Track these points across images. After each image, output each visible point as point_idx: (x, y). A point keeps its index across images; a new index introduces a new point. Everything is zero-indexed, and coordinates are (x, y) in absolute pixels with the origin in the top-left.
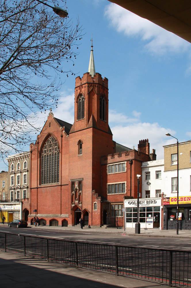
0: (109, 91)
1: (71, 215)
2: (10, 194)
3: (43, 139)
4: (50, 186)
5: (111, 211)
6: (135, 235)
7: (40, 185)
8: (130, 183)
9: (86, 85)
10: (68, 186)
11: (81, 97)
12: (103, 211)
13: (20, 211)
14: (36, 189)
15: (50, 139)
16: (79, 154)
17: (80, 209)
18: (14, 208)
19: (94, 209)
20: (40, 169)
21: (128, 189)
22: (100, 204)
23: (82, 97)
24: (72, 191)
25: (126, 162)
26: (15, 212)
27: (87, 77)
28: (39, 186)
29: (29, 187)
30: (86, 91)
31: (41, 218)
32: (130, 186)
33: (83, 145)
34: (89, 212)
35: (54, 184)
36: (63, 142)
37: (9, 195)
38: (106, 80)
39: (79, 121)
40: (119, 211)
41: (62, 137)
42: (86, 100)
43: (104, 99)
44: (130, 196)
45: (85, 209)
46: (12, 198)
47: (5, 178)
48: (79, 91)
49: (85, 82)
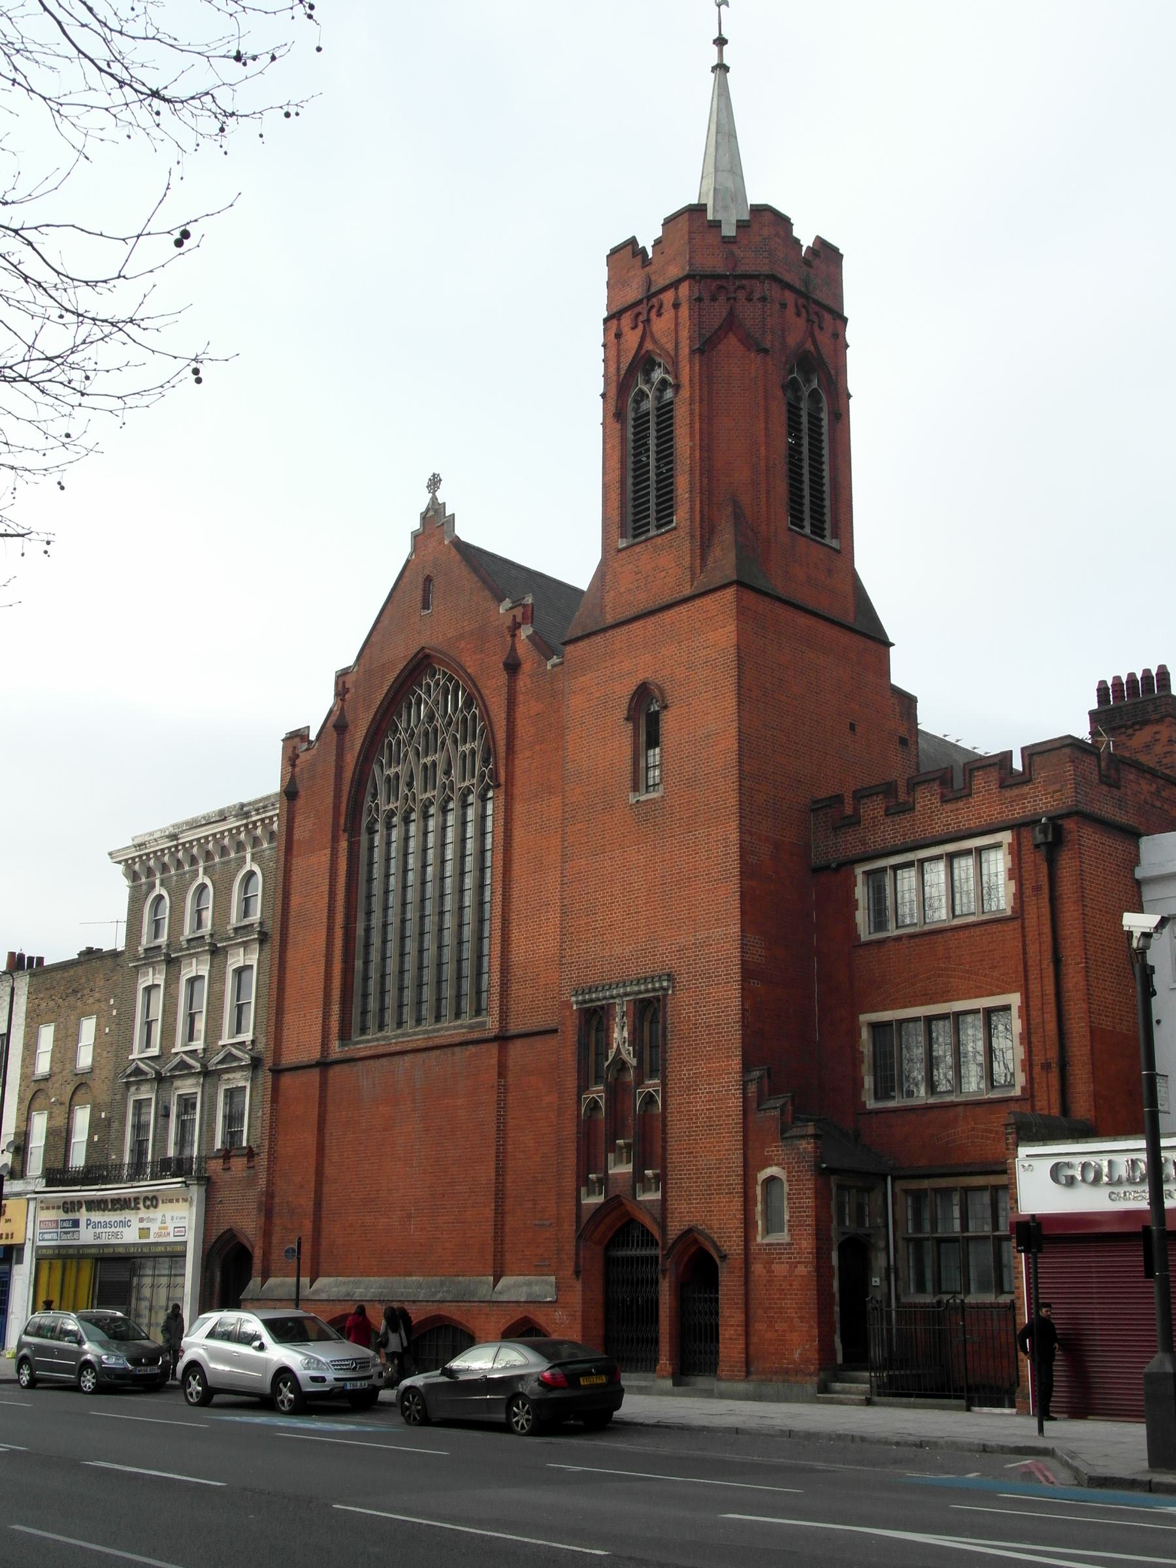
0: (850, 334)
1: (578, 1286)
4: (422, 1044)
5: (901, 1244)
6: (1150, 1487)
7: (345, 1036)
8: (1051, 1008)
9: (684, 289)
10: (552, 1042)
11: (648, 381)
12: (842, 1248)
13: (183, 1255)
14: (315, 1074)
15: (428, 692)
16: (635, 788)
17: (646, 1232)
18: (144, 1232)
19: (767, 1231)
21: (1038, 1059)
22: (809, 1185)
23: (657, 375)
25: (1006, 837)
26: (150, 1264)
27: (690, 240)
28: (336, 1050)
29: (269, 1062)
30: (684, 334)
31: (432, 1310)
32: (1052, 1026)
33: (669, 724)
34: (724, 1257)
35: (451, 1029)
36: (521, 710)
37: (115, 1125)
39: (638, 549)
40: (972, 1247)
41: (512, 667)
42: (685, 393)
43: (815, 384)
44: (1056, 1111)
45: (690, 1230)
46: (139, 1148)
47: (97, 995)
48: (632, 339)
49: (674, 272)
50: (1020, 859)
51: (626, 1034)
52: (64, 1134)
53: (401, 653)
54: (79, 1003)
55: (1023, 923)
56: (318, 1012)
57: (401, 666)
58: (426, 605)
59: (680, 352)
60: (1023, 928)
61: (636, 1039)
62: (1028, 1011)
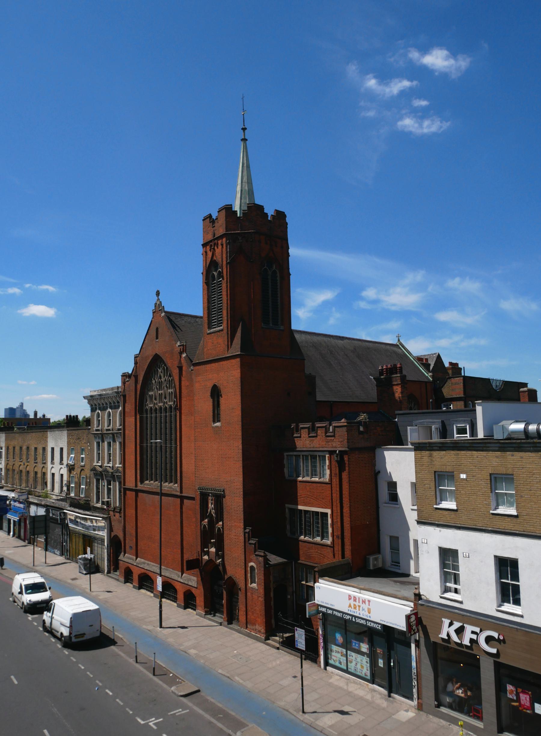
2: (93, 484)
3: (146, 367)
9: (224, 239)
20: (141, 442)
24: (202, 519)
38: (280, 216)
50: (331, 463)
51: (213, 506)
52: (79, 484)
53: (150, 354)
54: (80, 442)
55: (331, 486)
56: (134, 471)
57: (151, 358)
58: (157, 338)
59: (223, 263)
60: (332, 487)
61: (216, 508)
62: (333, 516)
